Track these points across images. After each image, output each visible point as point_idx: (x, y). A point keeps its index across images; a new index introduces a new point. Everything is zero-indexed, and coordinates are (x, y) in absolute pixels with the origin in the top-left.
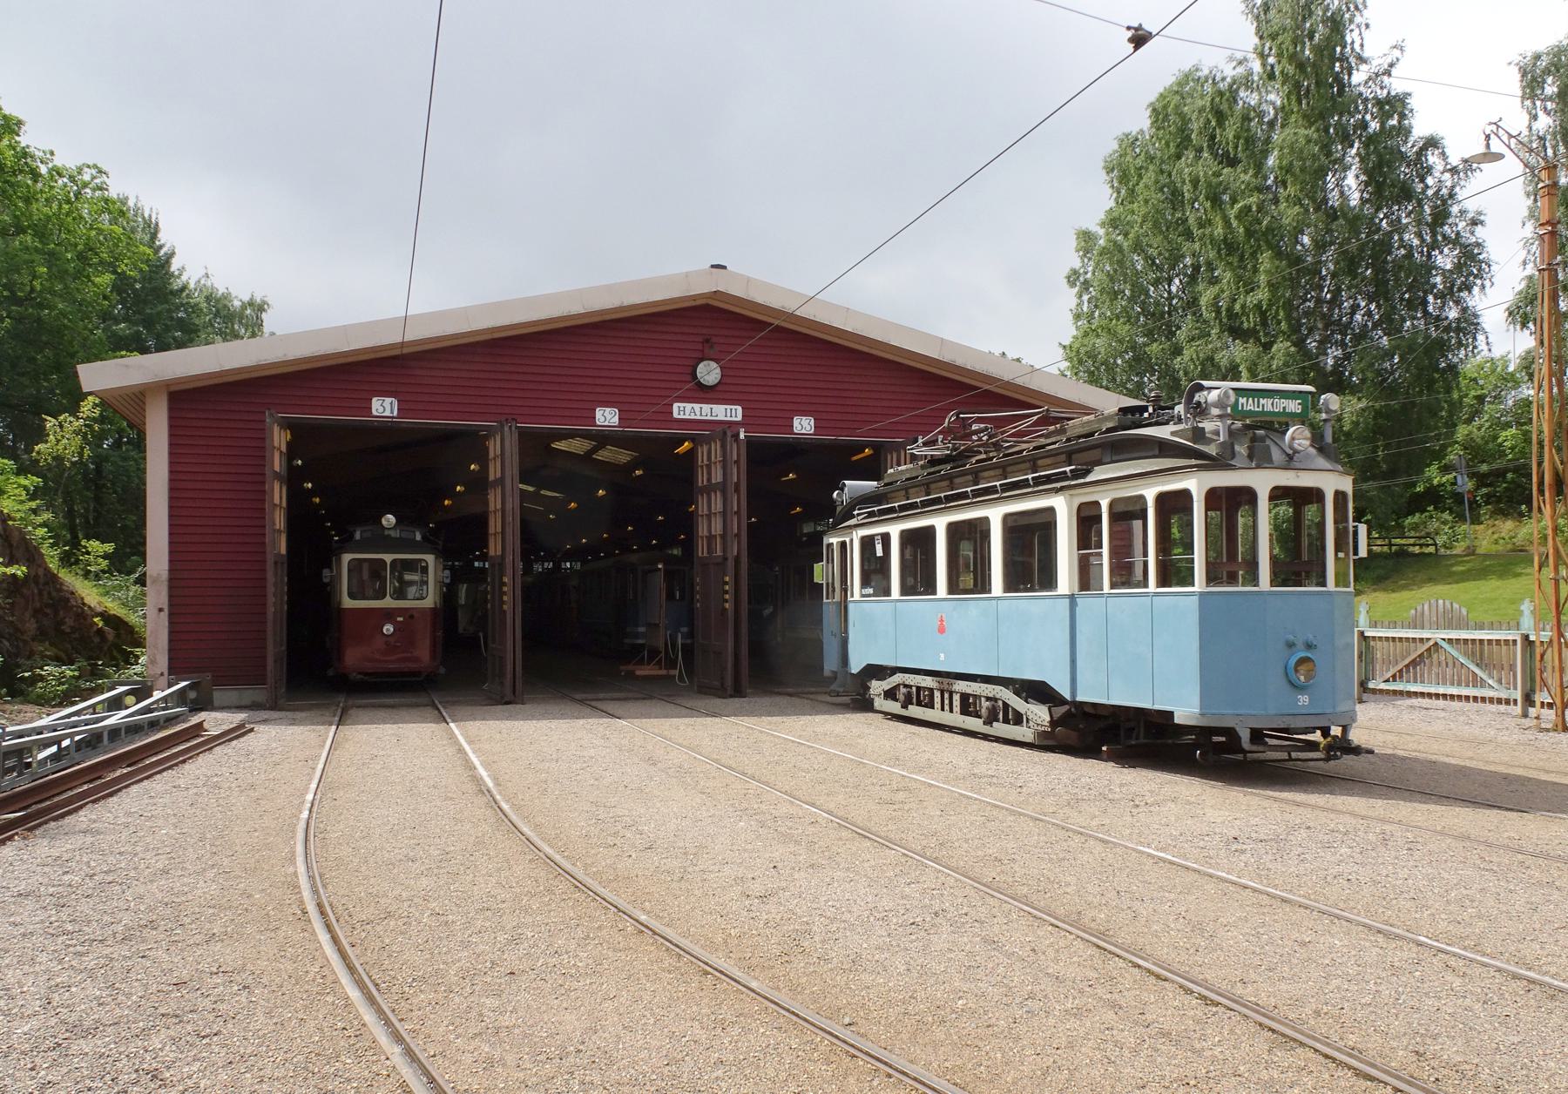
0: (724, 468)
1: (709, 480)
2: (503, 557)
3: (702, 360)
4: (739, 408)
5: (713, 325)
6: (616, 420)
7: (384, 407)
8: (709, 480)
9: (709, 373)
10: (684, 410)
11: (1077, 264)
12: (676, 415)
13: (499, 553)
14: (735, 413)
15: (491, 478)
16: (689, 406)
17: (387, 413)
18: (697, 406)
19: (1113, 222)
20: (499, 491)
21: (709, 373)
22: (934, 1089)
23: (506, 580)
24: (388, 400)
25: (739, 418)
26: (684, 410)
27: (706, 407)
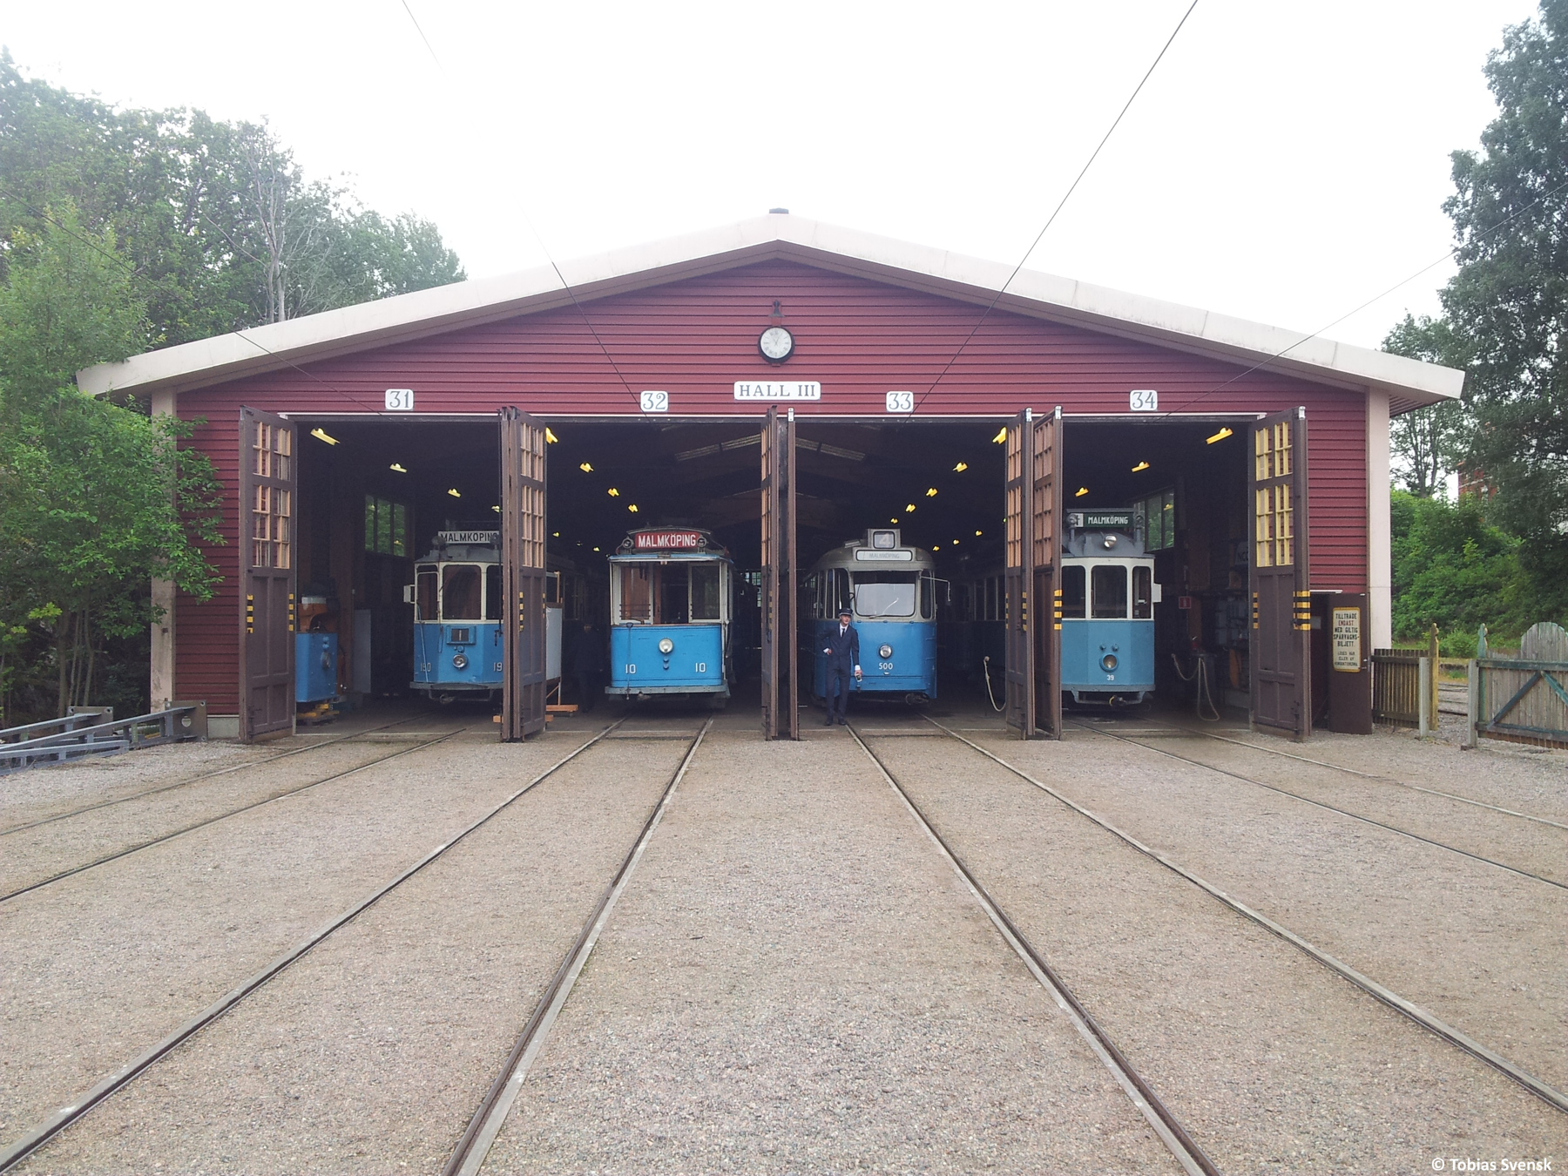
0: (1272, 460)
1: (1272, 470)
2: (1022, 569)
3: (770, 327)
4: (817, 385)
5: (780, 279)
6: (664, 406)
7: (399, 401)
8: (1272, 470)
9: (776, 343)
10: (748, 390)
11: (1453, 190)
12: (737, 396)
13: (1018, 564)
14: (811, 390)
15: (1011, 478)
16: (753, 385)
17: (402, 407)
18: (764, 384)
19: (1492, 138)
20: (1018, 492)
21: (776, 343)
22: (1204, 1166)
23: (1025, 595)
24: (403, 392)
25: (817, 396)
26: (748, 390)
27: (775, 386)
